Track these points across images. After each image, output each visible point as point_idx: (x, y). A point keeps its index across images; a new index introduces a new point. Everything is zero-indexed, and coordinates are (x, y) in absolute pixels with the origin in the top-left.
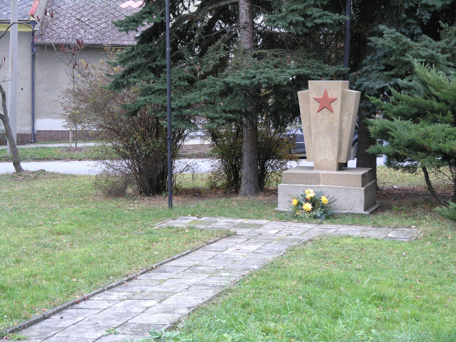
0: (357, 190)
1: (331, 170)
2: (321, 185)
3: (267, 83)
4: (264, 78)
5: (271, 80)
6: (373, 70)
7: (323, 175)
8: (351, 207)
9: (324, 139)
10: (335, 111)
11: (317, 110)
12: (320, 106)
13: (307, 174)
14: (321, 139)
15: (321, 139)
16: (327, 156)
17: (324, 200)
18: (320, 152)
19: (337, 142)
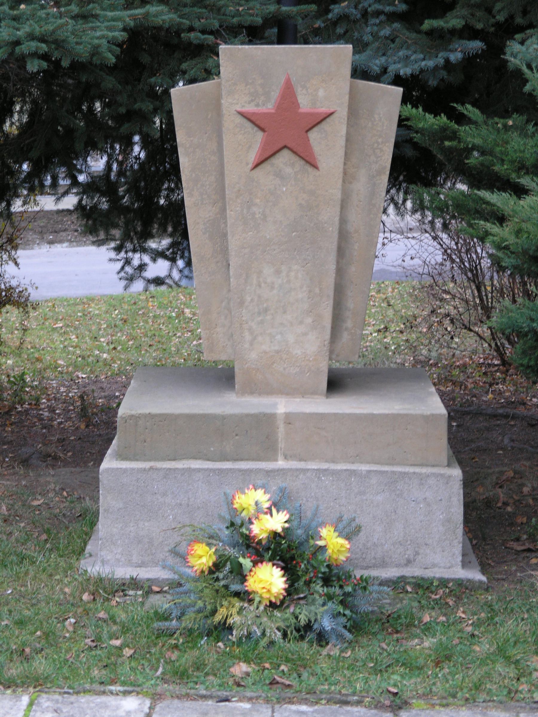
0: (431, 481)
1: (303, 392)
2: (281, 463)
3: (45, 57)
4: (31, 37)
5: (59, 44)
6: (365, 14)
7: (289, 418)
8: (410, 553)
9: (278, 272)
10: (322, 163)
11: (252, 157)
12: (265, 145)
13: (223, 418)
14: (268, 271)
15: (268, 271)
16: (291, 339)
17: (334, 543)
18: (262, 322)
19: (330, 281)
